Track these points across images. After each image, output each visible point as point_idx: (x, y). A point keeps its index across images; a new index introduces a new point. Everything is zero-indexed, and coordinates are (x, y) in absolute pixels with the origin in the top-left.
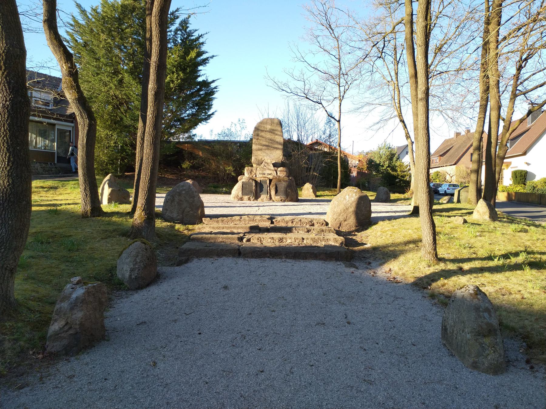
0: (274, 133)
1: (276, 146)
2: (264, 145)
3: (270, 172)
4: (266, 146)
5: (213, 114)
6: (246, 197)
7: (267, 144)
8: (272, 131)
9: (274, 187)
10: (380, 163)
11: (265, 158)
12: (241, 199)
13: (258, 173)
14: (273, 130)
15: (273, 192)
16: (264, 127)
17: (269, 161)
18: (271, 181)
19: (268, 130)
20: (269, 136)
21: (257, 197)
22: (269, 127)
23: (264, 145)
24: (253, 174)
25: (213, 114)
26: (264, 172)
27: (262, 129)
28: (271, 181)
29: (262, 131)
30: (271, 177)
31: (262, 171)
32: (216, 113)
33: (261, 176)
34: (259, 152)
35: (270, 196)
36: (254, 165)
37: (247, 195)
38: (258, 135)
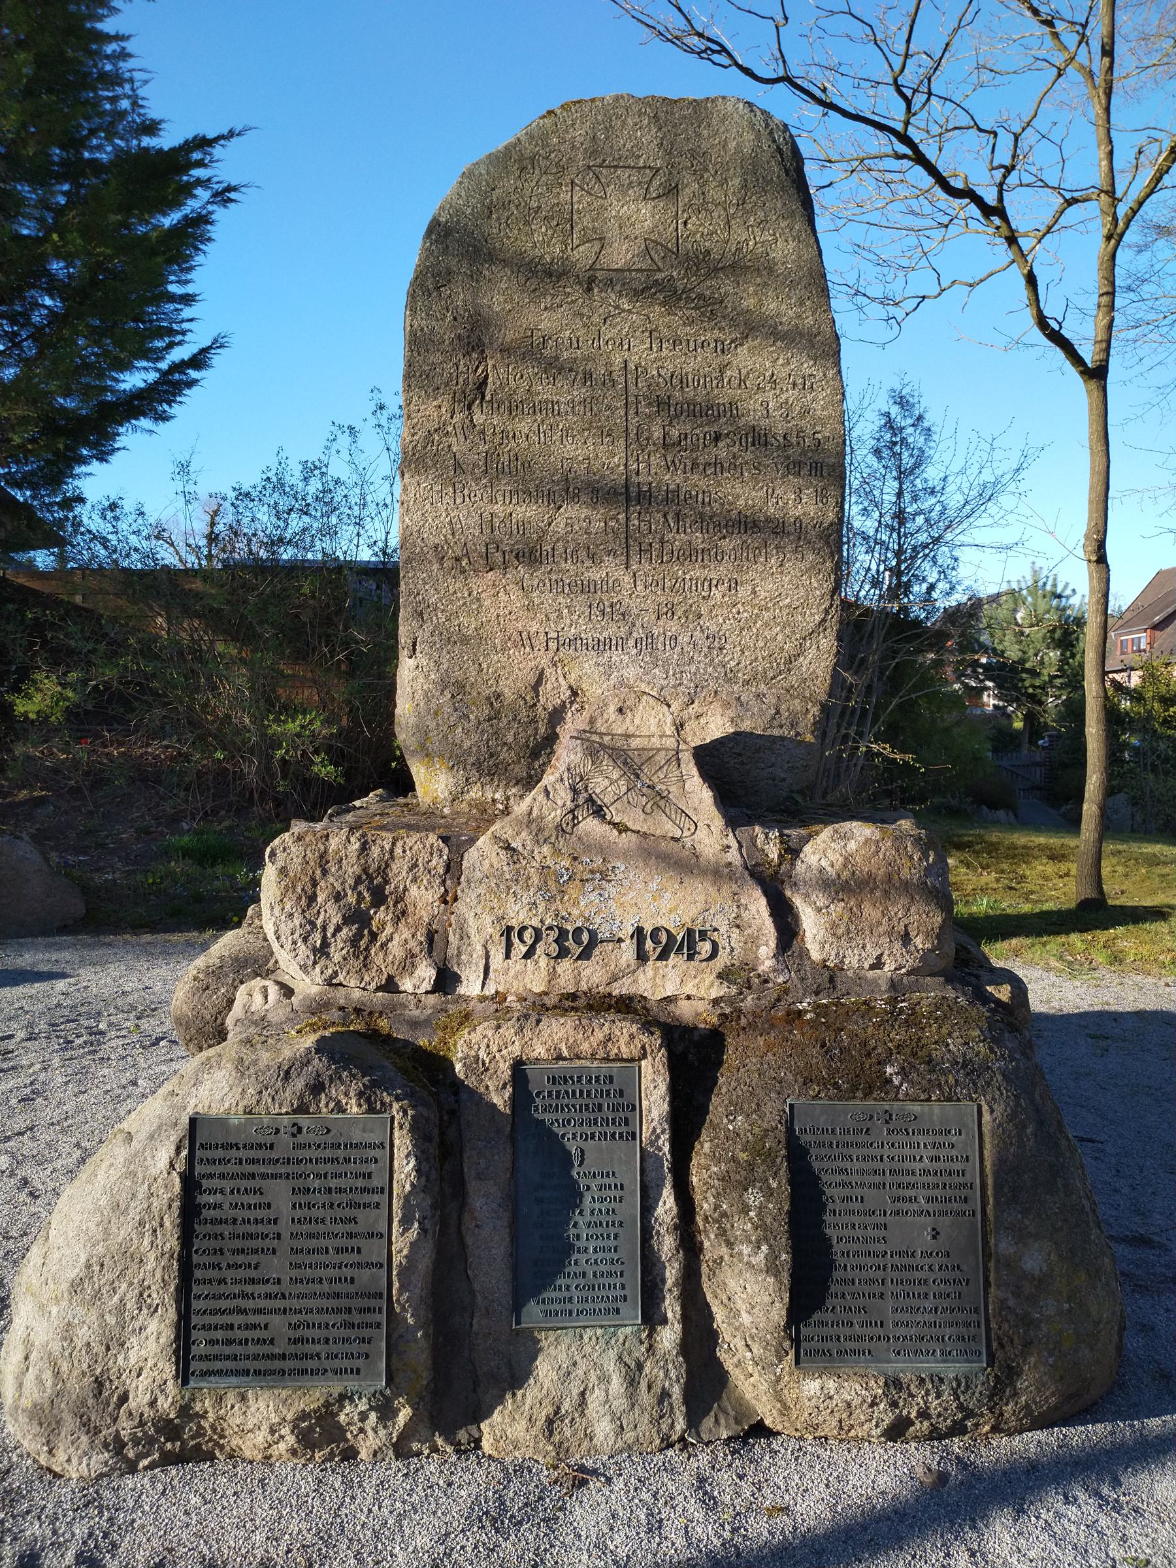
0: (710, 309)
1: (744, 494)
2: (569, 487)
3: (670, 905)
4: (598, 492)
5: (199, 361)
6: (257, 1418)
7: (611, 459)
8: (684, 282)
9: (767, 1201)
10: (1022, 661)
11: (587, 671)
12: (180, 1443)
13: (477, 921)
14: (702, 263)
15: (747, 1298)
16: (565, 221)
17: (650, 725)
18: (694, 1057)
19: (620, 255)
20: (640, 352)
21: (455, 1378)
22: (630, 221)
23: (569, 487)
24: (399, 939)
25: (199, 361)
26: (584, 906)
27: (540, 242)
28: (694, 1057)
29: (545, 276)
30: (689, 989)
31: (554, 886)
32: (217, 359)
33: (531, 976)
34: (500, 600)
35: (700, 1339)
36: (433, 783)
37: (270, 1368)
38: (475, 337)
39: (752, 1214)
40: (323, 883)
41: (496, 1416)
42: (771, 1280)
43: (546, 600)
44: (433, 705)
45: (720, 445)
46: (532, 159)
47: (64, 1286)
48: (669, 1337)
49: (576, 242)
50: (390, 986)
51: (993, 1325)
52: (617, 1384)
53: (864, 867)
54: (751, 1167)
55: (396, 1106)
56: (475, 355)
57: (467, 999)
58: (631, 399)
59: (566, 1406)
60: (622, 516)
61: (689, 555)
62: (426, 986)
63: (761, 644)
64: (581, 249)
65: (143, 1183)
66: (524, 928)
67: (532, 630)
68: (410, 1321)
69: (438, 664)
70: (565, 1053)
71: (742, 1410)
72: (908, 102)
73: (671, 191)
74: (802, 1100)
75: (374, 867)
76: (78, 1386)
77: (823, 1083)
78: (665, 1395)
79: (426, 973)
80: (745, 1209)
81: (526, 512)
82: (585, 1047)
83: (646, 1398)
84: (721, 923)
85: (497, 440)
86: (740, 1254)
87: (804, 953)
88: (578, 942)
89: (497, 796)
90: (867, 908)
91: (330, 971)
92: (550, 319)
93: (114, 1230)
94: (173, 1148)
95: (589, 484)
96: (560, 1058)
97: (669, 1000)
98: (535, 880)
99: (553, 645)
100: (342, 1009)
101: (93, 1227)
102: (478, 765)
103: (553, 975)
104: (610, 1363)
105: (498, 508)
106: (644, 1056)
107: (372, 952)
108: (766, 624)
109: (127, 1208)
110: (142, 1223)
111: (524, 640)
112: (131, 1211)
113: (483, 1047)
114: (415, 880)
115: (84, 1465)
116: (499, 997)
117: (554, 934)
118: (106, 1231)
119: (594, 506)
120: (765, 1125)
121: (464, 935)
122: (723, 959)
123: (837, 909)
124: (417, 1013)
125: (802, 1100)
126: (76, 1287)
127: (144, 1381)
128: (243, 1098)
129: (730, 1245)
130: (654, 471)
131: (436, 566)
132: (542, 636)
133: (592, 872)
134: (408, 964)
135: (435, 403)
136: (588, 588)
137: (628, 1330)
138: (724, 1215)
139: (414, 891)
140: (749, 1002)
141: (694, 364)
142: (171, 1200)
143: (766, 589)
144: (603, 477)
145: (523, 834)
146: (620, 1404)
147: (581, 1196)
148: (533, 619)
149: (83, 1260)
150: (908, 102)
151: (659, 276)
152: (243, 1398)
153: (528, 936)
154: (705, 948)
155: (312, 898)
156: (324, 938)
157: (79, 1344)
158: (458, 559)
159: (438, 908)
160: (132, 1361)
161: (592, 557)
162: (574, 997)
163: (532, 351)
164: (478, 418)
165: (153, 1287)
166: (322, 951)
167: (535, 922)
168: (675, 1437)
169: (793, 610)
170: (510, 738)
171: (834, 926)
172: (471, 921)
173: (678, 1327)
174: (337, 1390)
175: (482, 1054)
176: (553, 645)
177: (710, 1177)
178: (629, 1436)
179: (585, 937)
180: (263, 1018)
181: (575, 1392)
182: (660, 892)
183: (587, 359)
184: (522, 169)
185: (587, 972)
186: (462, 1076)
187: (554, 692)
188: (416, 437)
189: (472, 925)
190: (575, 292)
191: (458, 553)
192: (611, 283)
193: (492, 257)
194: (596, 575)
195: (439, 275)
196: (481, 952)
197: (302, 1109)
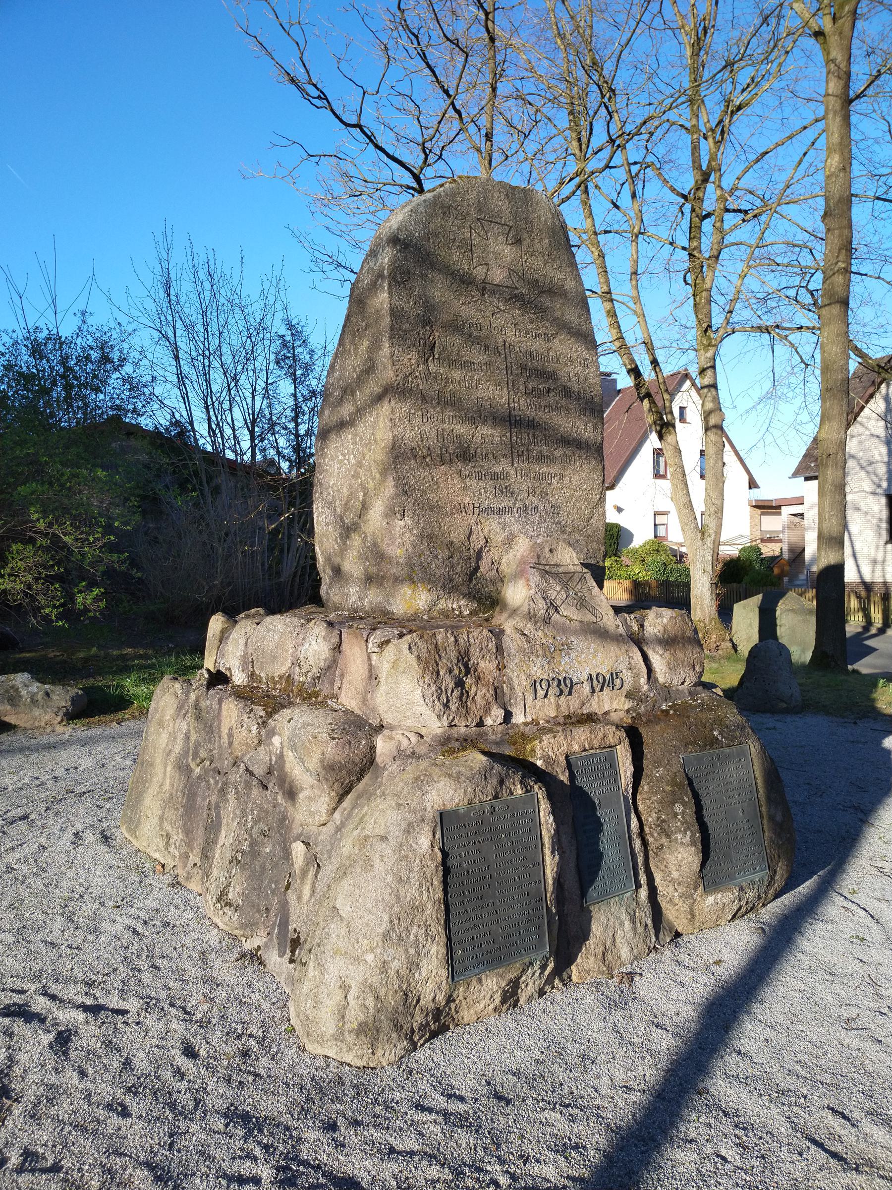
16: (468, 248)
20: (511, 335)
24: (480, 694)
38: (428, 316)
39: (679, 817)
40: (440, 663)
41: (579, 960)
42: (694, 849)
43: (471, 483)
44: (418, 549)
45: (551, 395)
46: (449, 208)
47: (378, 939)
48: (643, 893)
49: (475, 265)
50: (481, 724)
51: (768, 851)
52: (627, 924)
53: (672, 632)
54: (673, 792)
55: (536, 787)
56: (428, 328)
57: (517, 726)
58: (509, 364)
59: (608, 944)
60: (508, 434)
61: (542, 458)
62: (500, 720)
63: (575, 511)
64: (478, 269)
65: (415, 861)
66: (542, 680)
67: (466, 502)
68: (554, 911)
69: (418, 524)
70: (587, 747)
71: (671, 928)
72: (427, 156)
73: (518, 242)
74: (686, 755)
75: (463, 651)
76: (392, 1001)
77: (692, 743)
78: (646, 925)
79: (498, 713)
80: (676, 815)
81: (461, 429)
82: (596, 743)
83: (640, 929)
84: (623, 667)
85: (443, 384)
86: (676, 839)
87: (656, 679)
88: (565, 686)
89: (454, 606)
90: (678, 652)
91: (451, 717)
92: (466, 308)
93: (402, 895)
94: (431, 834)
95: (491, 414)
96: (585, 750)
97: (606, 713)
98: (540, 652)
99: (476, 511)
100: (457, 740)
101: (387, 897)
102: (444, 587)
103: (558, 706)
104: (624, 917)
105: (446, 426)
106: (620, 743)
107: (469, 703)
108: (577, 500)
109: (408, 878)
110: (421, 886)
111: (462, 509)
112: (413, 880)
113: (550, 750)
114: (483, 658)
115: (393, 1054)
116: (535, 722)
117: (555, 683)
118: (397, 897)
119: (494, 426)
120: (675, 770)
121: (512, 688)
122: (626, 687)
123: (667, 654)
124: (494, 737)
125: (686, 755)
126: (386, 936)
127: (430, 986)
128: (466, 795)
129: (668, 836)
130: (523, 405)
131: (413, 462)
132: (471, 506)
133: (562, 645)
134: (487, 710)
135: (408, 357)
136: (495, 477)
137: (628, 894)
138: (664, 821)
139: (482, 664)
140: (642, 709)
141: (537, 346)
142: (437, 867)
143: (576, 478)
144: (498, 410)
145: (529, 625)
146: (630, 935)
147: (602, 825)
148: (466, 495)
149: (386, 918)
150: (427, 156)
151: (517, 292)
152: (480, 980)
153: (544, 685)
154: (618, 682)
155: (438, 673)
156: (447, 697)
157: (392, 973)
158: (424, 457)
159: (496, 673)
160: (424, 975)
161: (495, 458)
162: (569, 717)
163: (456, 326)
164: (432, 368)
165: (432, 925)
166: (446, 706)
167: (545, 676)
168: (652, 947)
169: (588, 492)
170: (459, 570)
171: (669, 664)
172: (515, 679)
173: (646, 887)
174: (527, 960)
175: (550, 753)
176: (476, 511)
177: (652, 803)
178: (635, 951)
179: (568, 682)
180: (413, 753)
181: (611, 935)
182: (596, 651)
183: (486, 338)
184: (444, 213)
185: (573, 701)
186: (544, 768)
187: (477, 542)
188: (399, 378)
189: (516, 681)
190: (476, 293)
191: (425, 453)
192: (493, 292)
193: (432, 266)
194: (498, 469)
195: (404, 273)
196: (522, 697)
197: (496, 797)
